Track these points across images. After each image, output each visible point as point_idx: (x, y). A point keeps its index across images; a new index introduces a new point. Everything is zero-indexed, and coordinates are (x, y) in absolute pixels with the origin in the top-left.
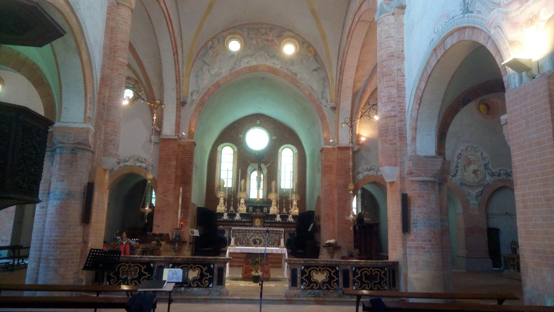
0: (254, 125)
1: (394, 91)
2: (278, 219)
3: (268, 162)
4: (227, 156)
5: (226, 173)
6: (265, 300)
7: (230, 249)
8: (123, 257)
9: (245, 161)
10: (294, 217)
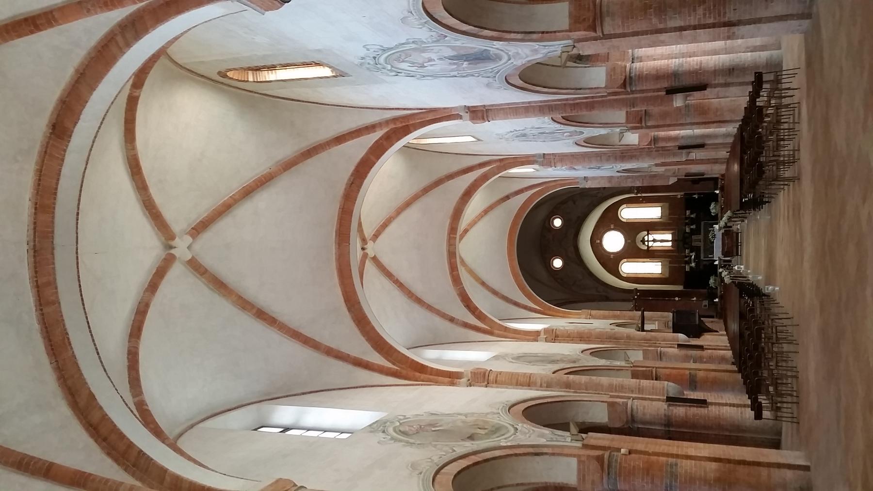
0: (601, 244)
1: (629, 180)
2: (693, 227)
3: (632, 229)
4: (629, 268)
5: (653, 268)
6: (722, 163)
9: (633, 252)
10: (691, 213)
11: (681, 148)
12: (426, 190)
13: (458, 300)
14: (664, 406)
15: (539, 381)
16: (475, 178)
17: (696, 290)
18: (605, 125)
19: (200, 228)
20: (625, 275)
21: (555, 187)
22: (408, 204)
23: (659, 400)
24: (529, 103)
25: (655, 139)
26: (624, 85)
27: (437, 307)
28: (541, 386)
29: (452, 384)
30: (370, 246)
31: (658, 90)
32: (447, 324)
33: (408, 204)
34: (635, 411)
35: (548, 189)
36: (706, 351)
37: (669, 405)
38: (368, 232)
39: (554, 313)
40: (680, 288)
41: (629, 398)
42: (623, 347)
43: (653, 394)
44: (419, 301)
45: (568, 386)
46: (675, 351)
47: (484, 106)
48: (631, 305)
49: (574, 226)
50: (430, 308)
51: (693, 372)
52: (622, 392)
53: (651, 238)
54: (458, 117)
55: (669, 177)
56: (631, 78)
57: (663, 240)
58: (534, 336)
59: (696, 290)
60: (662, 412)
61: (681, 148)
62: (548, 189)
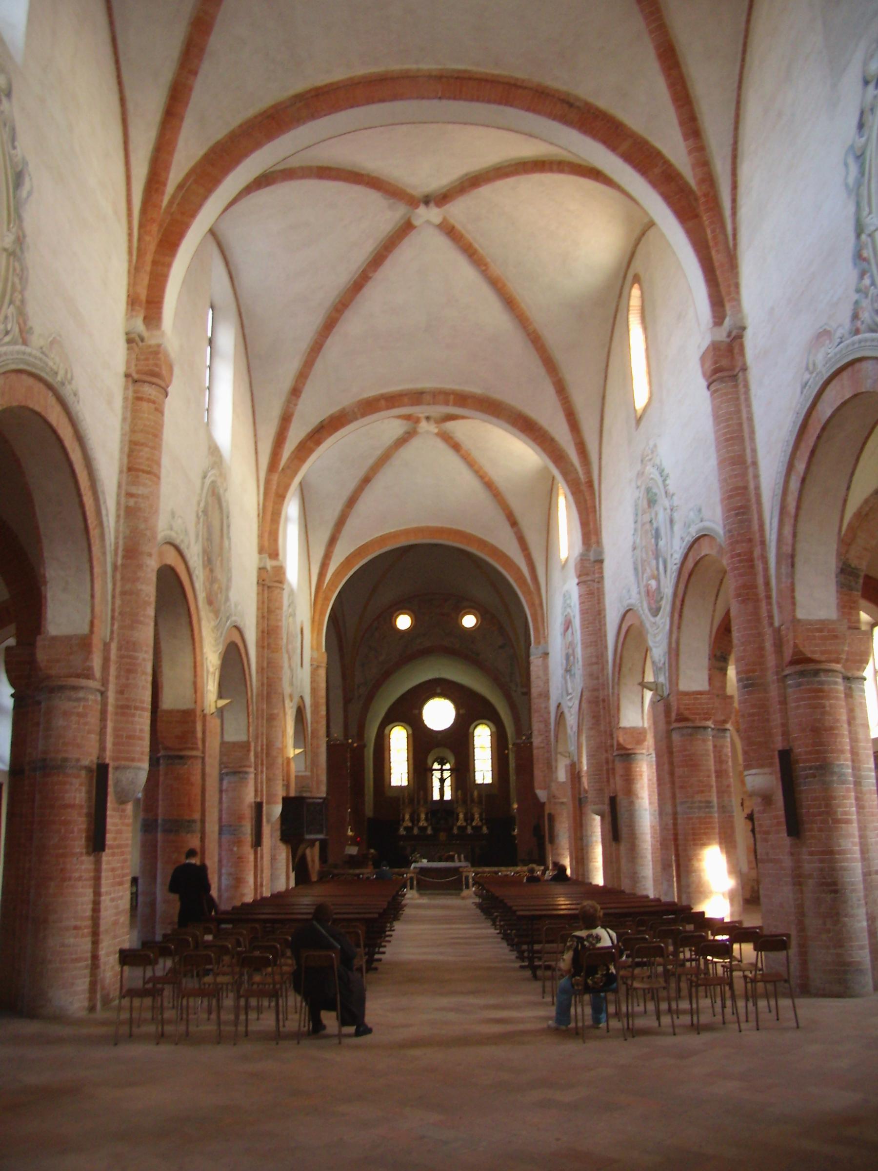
1: (542, 726)
3: (457, 743)
4: (399, 739)
5: (399, 774)
7: (676, 900)
8: (121, 898)
9: (424, 745)
11: (613, 801)
12: (536, 341)
13: (333, 409)
14: (89, 759)
15: (140, 490)
16: (557, 437)
17: (362, 834)
18: (674, 652)
19: (450, 231)
20: (386, 731)
21: (532, 605)
22: (510, 303)
23: (102, 748)
24: (755, 464)
25: (629, 755)
26: (800, 659)
27: (319, 365)
28: (129, 495)
29: (133, 301)
30: (433, 428)
31: (786, 734)
32: (287, 384)
33: (510, 303)
34: (73, 694)
35: (527, 593)
36: (252, 852)
37: (88, 769)
38: (450, 425)
39: (319, 606)
40: (369, 810)
41: (105, 682)
42: (253, 708)
43: (116, 736)
44: (329, 325)
45: (132, 552)
46: (250, 797)
47: (744, 369)
48: (338, 733)
49: (463, 648)
50: (316, 348)
51: (198, 825)
52: (119, 669)
53: (447, 774)
54: (719, 317)
55: (547, 787)
56: (816, 673)
57: (442, 786)
58: (269, 546)
59: (362, 834)
60: (73, 754)
61: (613, 801)
62: (527, 593)
